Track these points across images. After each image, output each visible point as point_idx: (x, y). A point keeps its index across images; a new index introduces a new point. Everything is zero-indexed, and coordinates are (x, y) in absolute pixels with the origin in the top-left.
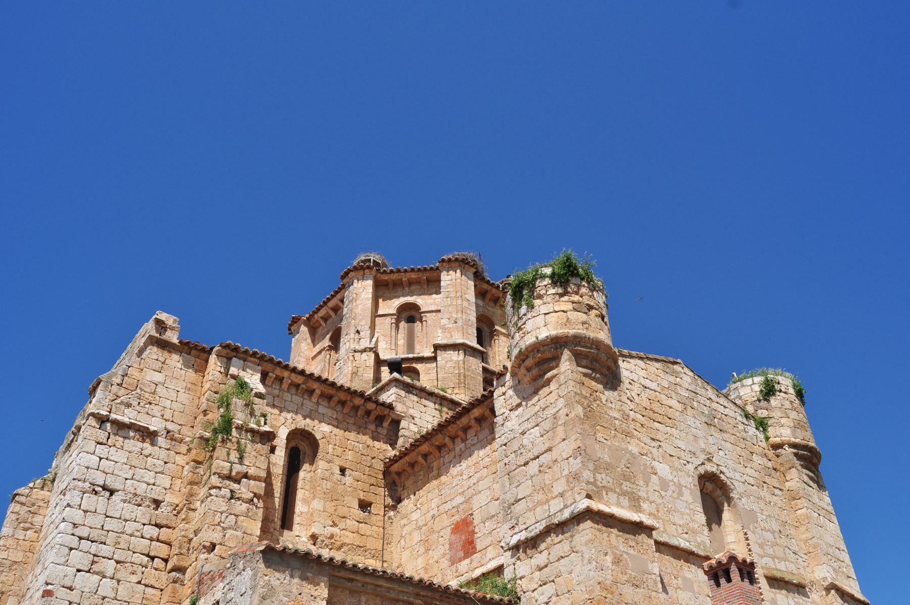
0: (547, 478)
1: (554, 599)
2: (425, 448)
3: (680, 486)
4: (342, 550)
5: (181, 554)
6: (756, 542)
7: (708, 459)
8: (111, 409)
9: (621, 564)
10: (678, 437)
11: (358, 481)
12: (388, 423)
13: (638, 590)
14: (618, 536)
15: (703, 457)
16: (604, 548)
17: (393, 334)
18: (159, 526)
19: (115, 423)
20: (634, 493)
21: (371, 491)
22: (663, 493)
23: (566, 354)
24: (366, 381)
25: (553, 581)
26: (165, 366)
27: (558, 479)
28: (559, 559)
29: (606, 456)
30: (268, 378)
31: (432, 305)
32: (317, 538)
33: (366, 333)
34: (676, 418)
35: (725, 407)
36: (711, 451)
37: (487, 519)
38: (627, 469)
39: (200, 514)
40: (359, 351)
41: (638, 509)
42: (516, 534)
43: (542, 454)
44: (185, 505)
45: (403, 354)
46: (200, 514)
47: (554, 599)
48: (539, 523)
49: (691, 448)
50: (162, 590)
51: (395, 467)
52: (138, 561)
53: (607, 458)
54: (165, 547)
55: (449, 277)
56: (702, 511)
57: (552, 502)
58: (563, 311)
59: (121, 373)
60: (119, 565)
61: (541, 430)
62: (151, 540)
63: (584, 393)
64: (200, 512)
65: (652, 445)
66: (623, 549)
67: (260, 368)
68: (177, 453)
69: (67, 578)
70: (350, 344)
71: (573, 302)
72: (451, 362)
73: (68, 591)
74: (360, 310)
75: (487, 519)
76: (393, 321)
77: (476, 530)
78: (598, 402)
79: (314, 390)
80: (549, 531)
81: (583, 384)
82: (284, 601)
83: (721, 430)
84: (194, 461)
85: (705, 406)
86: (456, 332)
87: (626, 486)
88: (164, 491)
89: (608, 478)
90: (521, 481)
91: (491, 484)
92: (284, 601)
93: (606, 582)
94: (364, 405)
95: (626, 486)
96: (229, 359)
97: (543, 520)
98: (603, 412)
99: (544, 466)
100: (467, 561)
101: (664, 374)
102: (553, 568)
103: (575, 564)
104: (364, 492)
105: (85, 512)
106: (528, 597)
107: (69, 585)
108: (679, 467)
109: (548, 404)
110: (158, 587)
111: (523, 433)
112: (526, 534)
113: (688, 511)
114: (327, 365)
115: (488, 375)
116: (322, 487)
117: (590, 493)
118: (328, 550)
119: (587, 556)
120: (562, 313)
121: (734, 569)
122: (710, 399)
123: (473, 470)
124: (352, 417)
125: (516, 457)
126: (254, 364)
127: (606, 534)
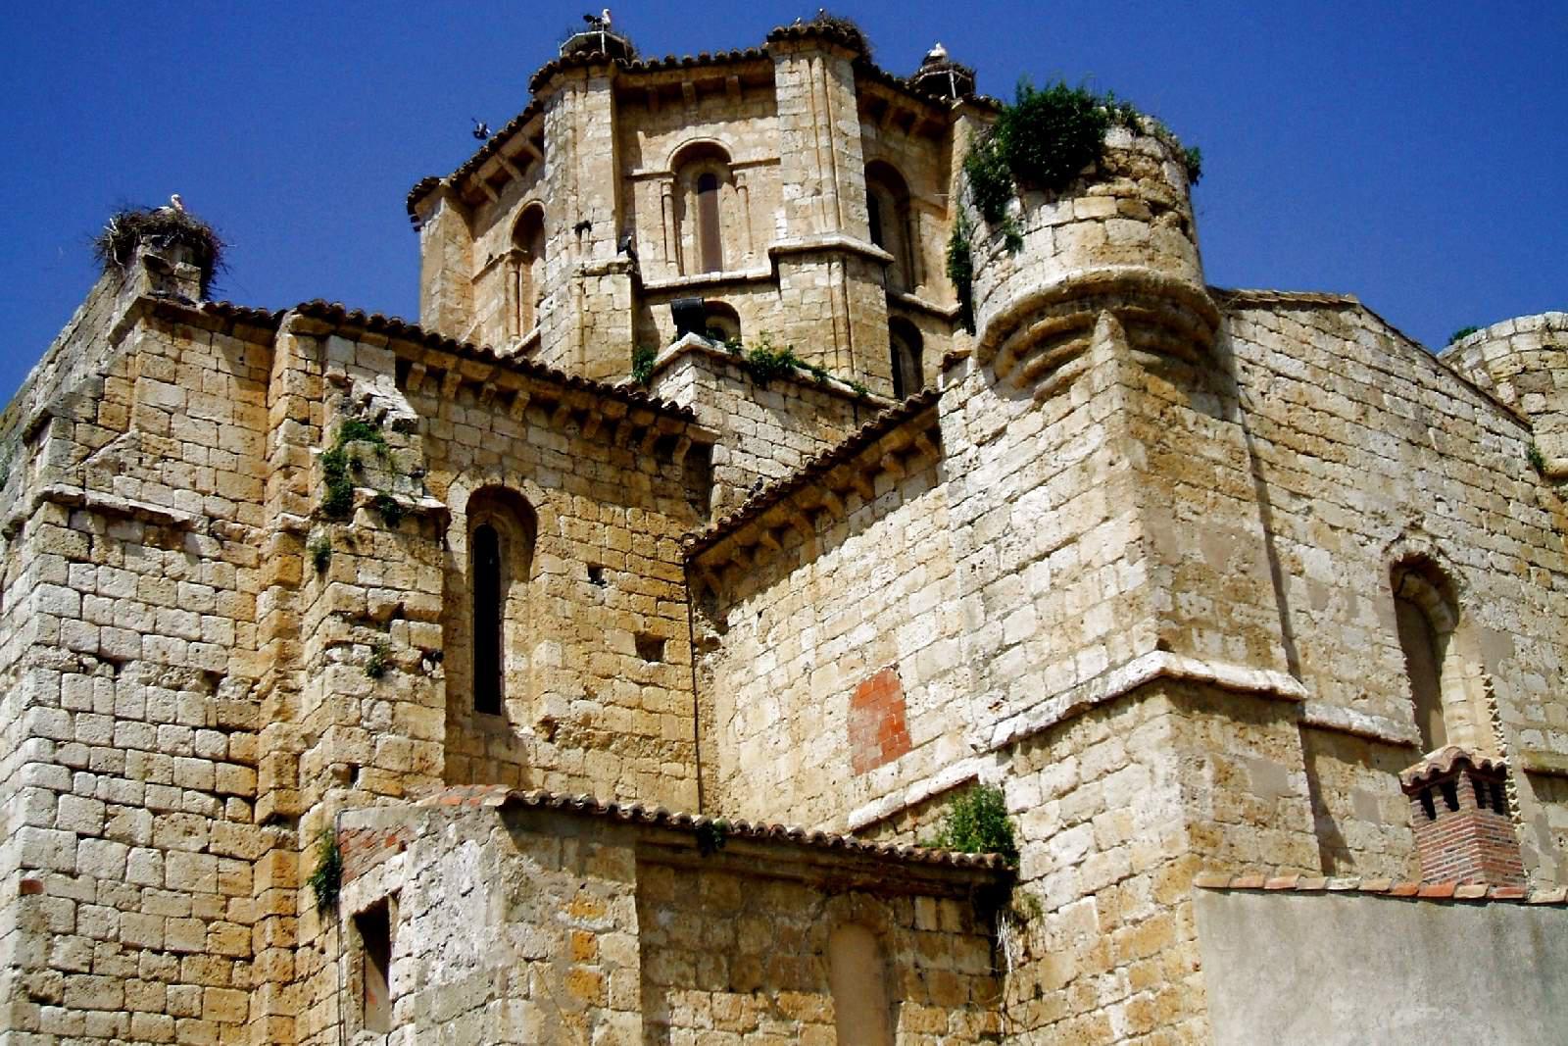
0: (1071, 601)
1: (1092, 856)
2: (777, 515)
3: (1351, 595)
4: (613, 747)
5: (283, 787)
6: (1510, 700)
7: (1413, 524)
8: (84, 481)
9: (1232, 782)
10: (1349, 482)
11: (630, 593)
12: (684, 453)
13: (1266, 832)
14: (1223, 724)
15: (1401, 521)
16: (1198, 751)
17: (669, 223)
18: (225, 729)
19: (100, 510)
20: (1256, 626)
21: (660, 613)
22: (1316, 615)
23: (1104, 325)
24: (616, 345)
25: (1090, 820)
26: (180, 367)
27: (1094, 606)
28: (1099, 777)
29: (1198, 551)
30: (411, 376)
31: (755, 146)
32: (557, 728)
33: (605, 228)
34: (1343, 439)
35: (1451, 397)
36: (1420, 505)
37: (934, 677)
38: (1241, 576)
39: (312, 702)
40: (593, 274)
41: (1264, 660)
42: (1002, 720)
43: (1057, 549)
44: (274, 683)
45: (697, 273)
46: (312, 702)
47: (1092, 856)
48: (1055, 700)
49: (1374, 505)
50: (252, 862)
51: (711, 556)
52: (194, 806)
53: (1199, 557)
54: (247, 771)
55: (795, 79)
56: (1397, 644)
57: (1082, 656)
58: (1096, 219)
59: (90, 395)
60: (158, 819)
61: (1053, 495)
62: (215, 760)
63: (1147, 410)
64: (311, 696)
65: (1294, 508)
66: (1235, 752)
67: (391, 354)
68: (238, 566)
69: (60, 854)
70: (570, 256)
71: (1117, 197)
72: (813, 292)
73: (69, 879)
74: (586, 169)
75: (934, 677)
76: (667, 191)
77: (909, 701)
78: (1178, 428)
79: (514, 393)
80: (1075, 715)
81: (1145, 389)
82: (554, 904)
83: (1441, 455)
84: (278, 582)
85: (1409, 400)
86: (822, 217)
87: (1241, 613)
88: (224, 653)
89: (1203, 599)
90: (1010, 607)
91: (937, 602)
92: (554, 904)
93: (1203, 823)
94: (627, 417)
95: (1241, 613)
96: (321, 340)
97: (1063, 692)
98: (1189, 449)
99: (1063, 575)
100: (891, 767)
101: (1319, 337)
102: (1089, 794)
103: (1135, 786)
104: (645, 615)
105: (73, 712)
106: (1035, 852)
107: (68, 867)
108: (1351, 551)
109: (1068, 438)
110: (243, 856)
111: (1011, 500)
112: (1027, 721)
113: (1367, 648)
114: (512, 298)
115: (897, 313)
116: (554, 615)
117: (1165, 637)
118: (581, 749)
119: (1161, 772)
120: (1093, 223)
121: (1463, 782)
122: (1418, 382)
123: (892, 569)
124: (602, 446)
125: (998, 552)
126: (378, 346)
127: (1200, 723)
